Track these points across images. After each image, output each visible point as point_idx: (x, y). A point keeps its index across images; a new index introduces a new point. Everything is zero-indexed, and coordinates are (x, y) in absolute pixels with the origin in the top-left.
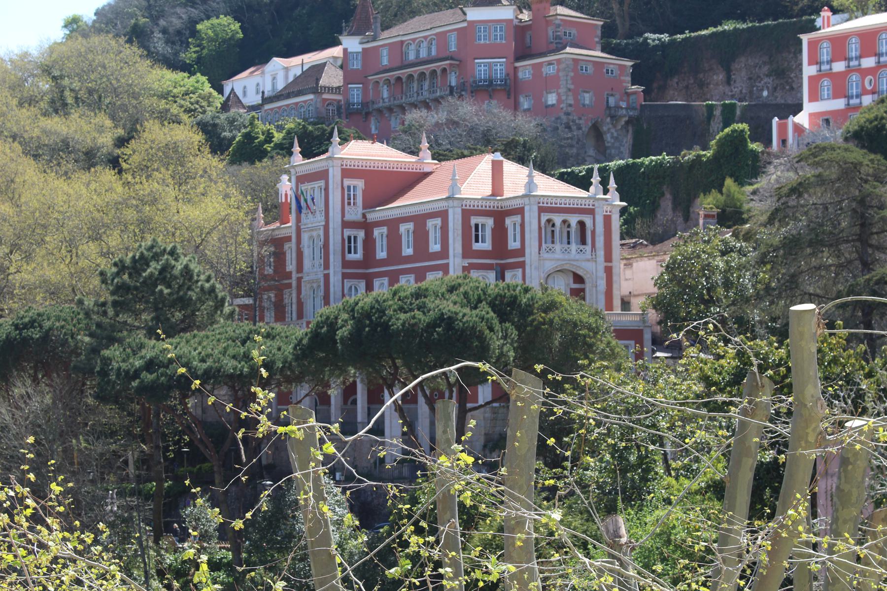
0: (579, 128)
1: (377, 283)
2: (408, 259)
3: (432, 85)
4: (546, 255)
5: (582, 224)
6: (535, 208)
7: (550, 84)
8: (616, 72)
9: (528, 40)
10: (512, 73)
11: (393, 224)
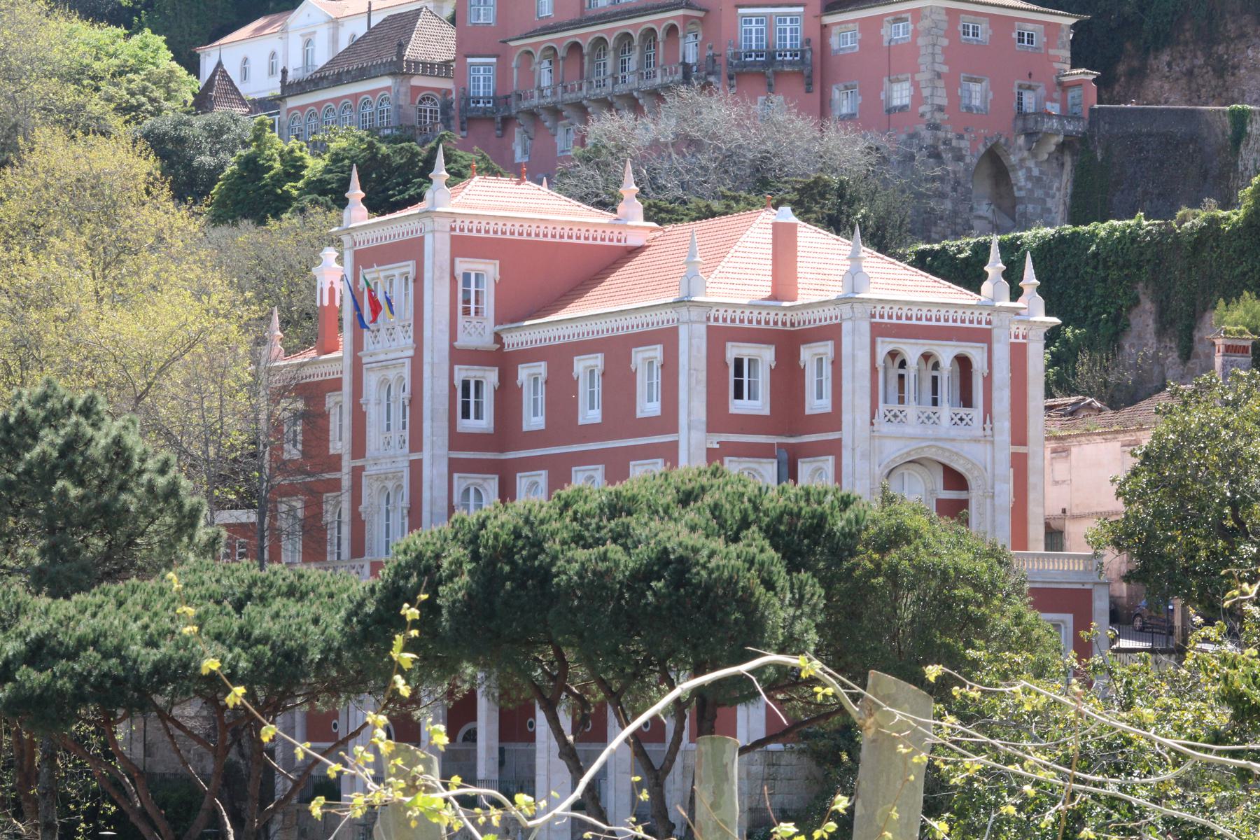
0: (959, 157)
1: (522, 481)
3: (646, 61)
4: (883, 427)
5: (963, 363)
6: (865, 327)
8: (1040, 39)
11: (559, 357)
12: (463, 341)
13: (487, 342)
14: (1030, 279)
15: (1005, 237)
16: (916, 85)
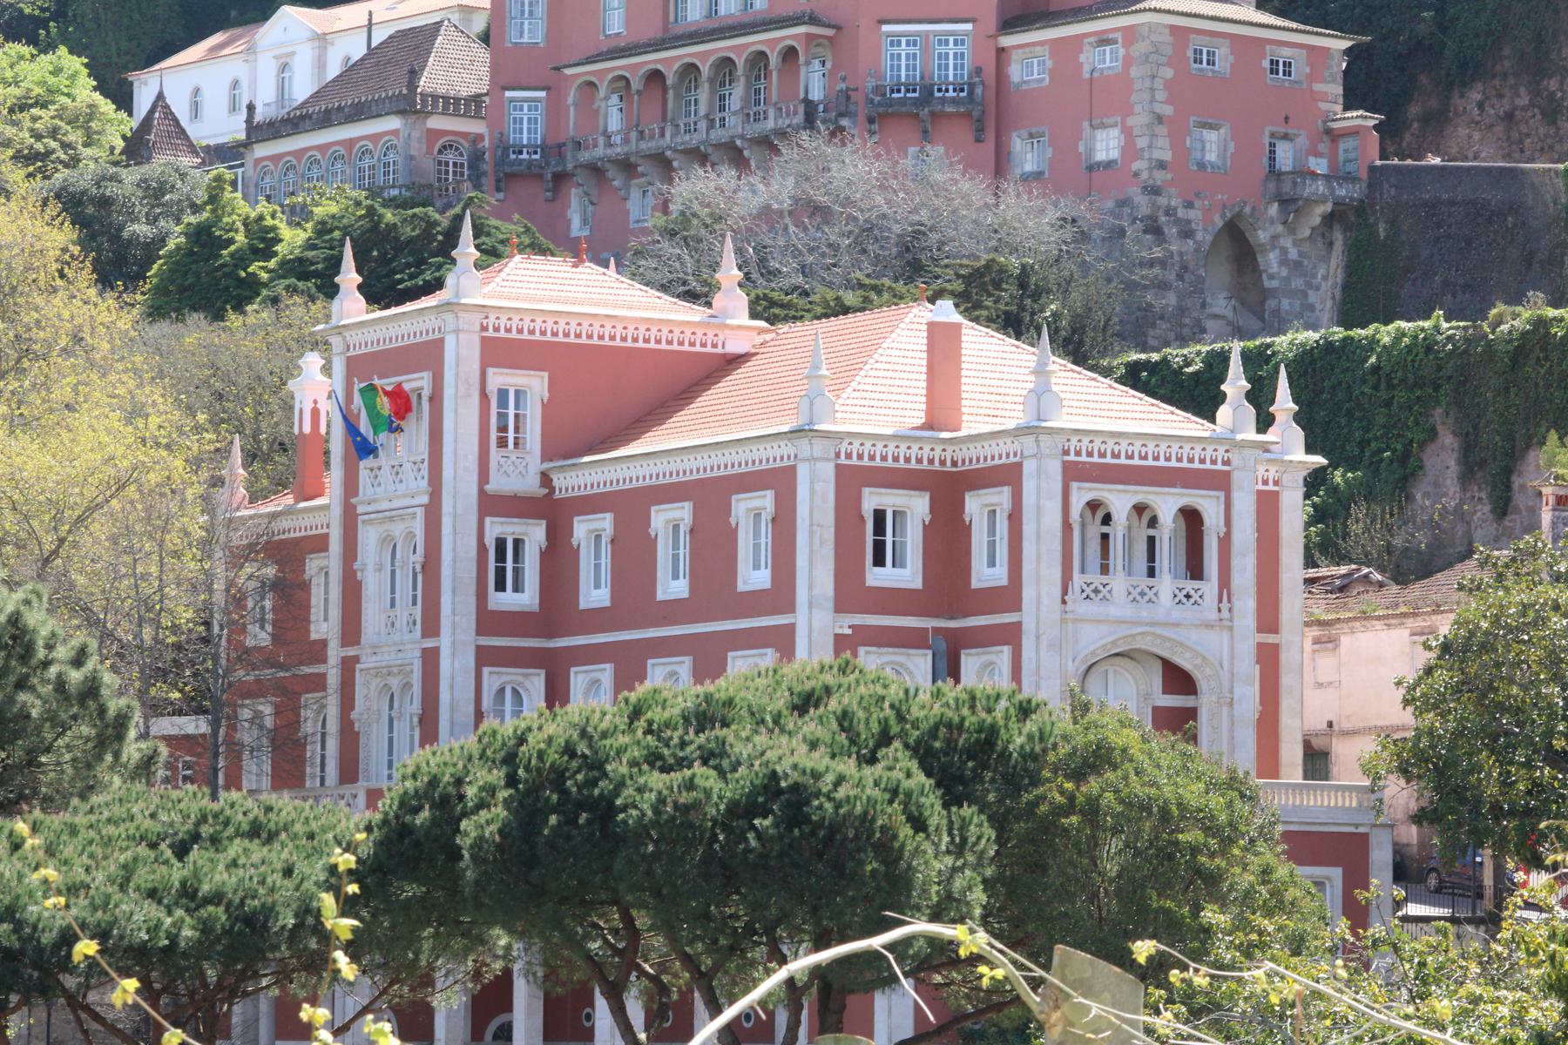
0: (1187, 233)
1: (579, 679)
3: (754, 97)
5: (1191, 518)
6: (1055, 468)
8: (1300, 69)
12: (497, 484)
13: (528, 484)
14: (1284, 402)
16: (1128, 133)
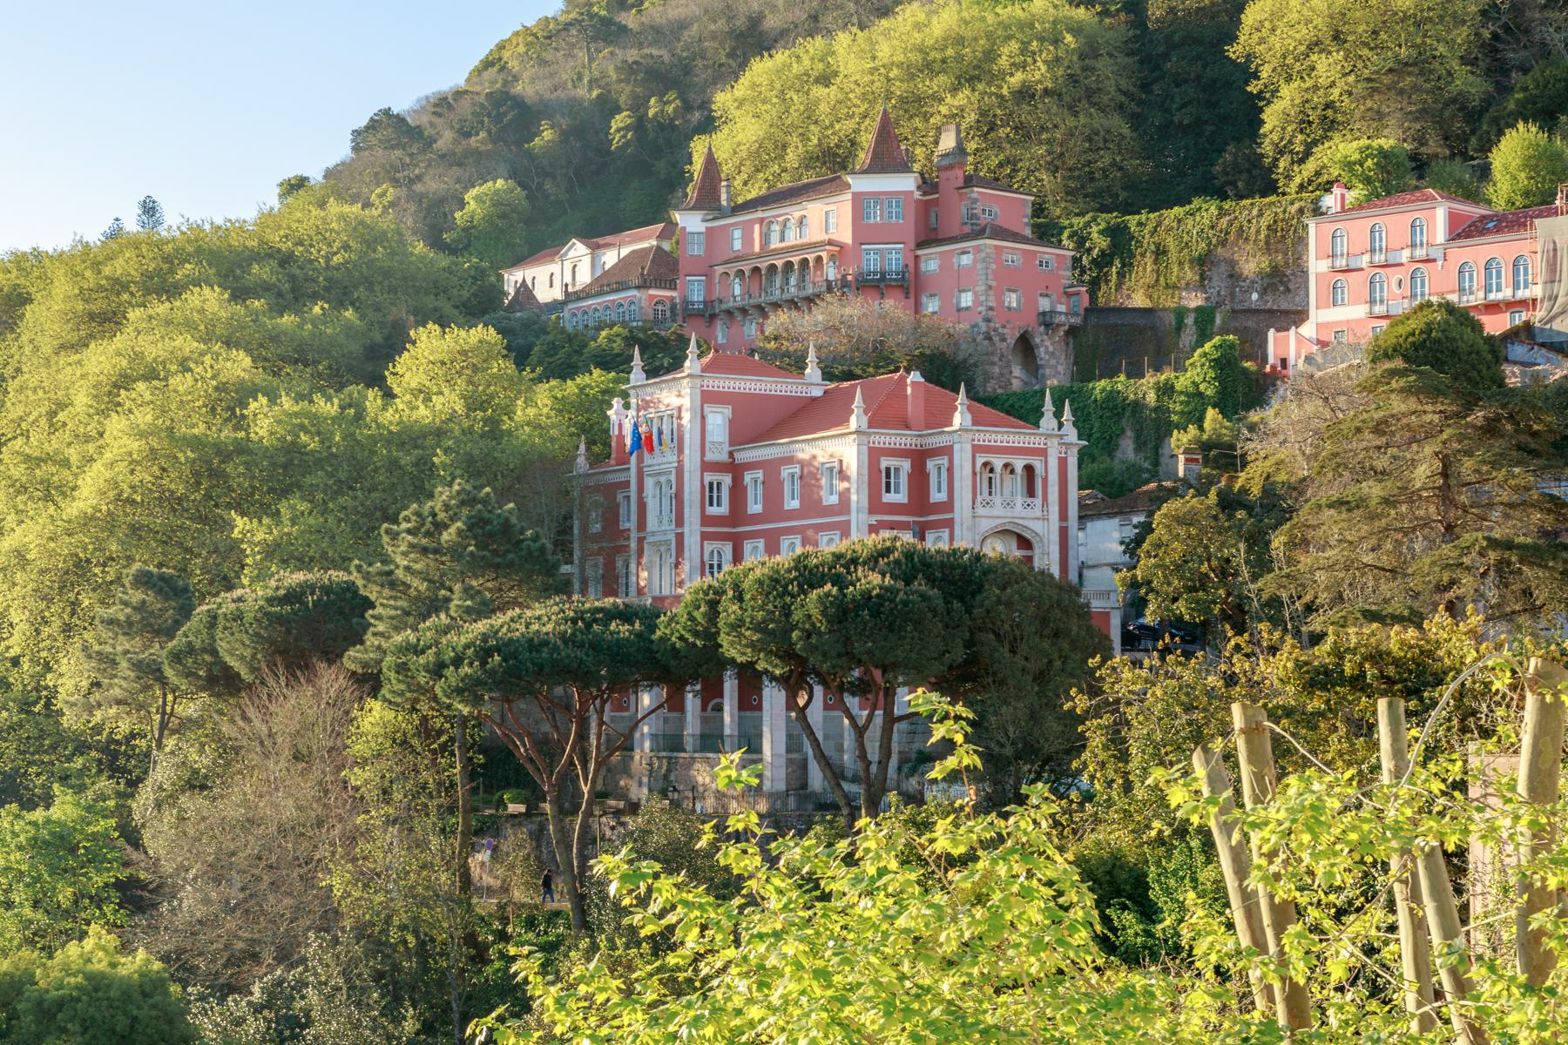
0: (1003, 340)
1: (748, 546)
2: (792, 515)
3: (802, 279)
4: (981, 511)
5: (1029, 469)
6: (968, 448)
7: (961, 281)
8: (1053, 265)
9: (933, 220)
10: (911, 265)
11: (771, 468)
12: (709, 457)
13: (723, 457)
14: (1067, 414)
15: (571, 387)
16: (976, 294)
